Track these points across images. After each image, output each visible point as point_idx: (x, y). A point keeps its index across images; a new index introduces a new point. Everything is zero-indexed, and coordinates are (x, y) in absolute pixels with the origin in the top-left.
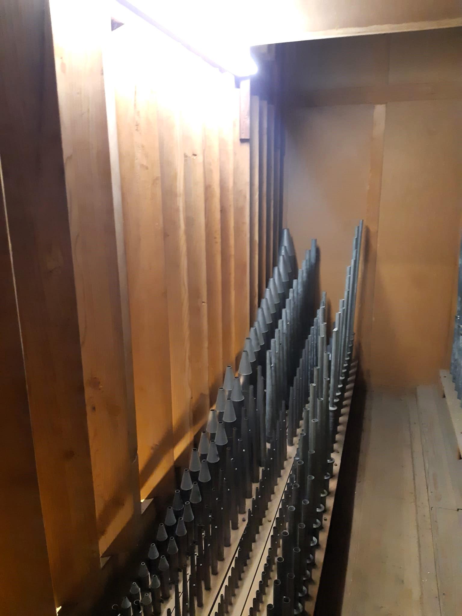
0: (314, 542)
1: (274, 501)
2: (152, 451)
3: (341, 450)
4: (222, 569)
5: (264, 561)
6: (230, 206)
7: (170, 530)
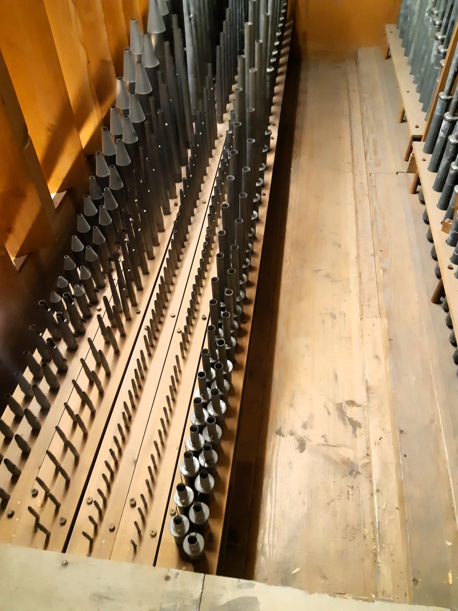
0: (254, 216)
1: (207, 183)
2: (50, 133)
3: (277, 122)
4: (159, 254)
5: (203, 240)
7: (93, 220)
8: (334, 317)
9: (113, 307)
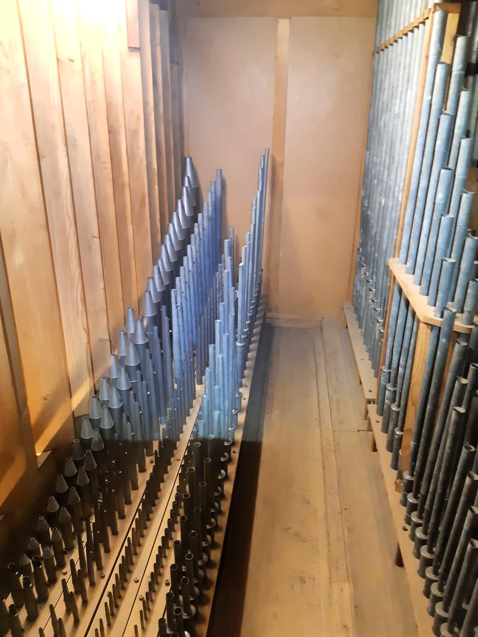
3: (249, 385)
4: (130, 513)
7: (71, 481)
8: (303, 580)
9: (79, 570)
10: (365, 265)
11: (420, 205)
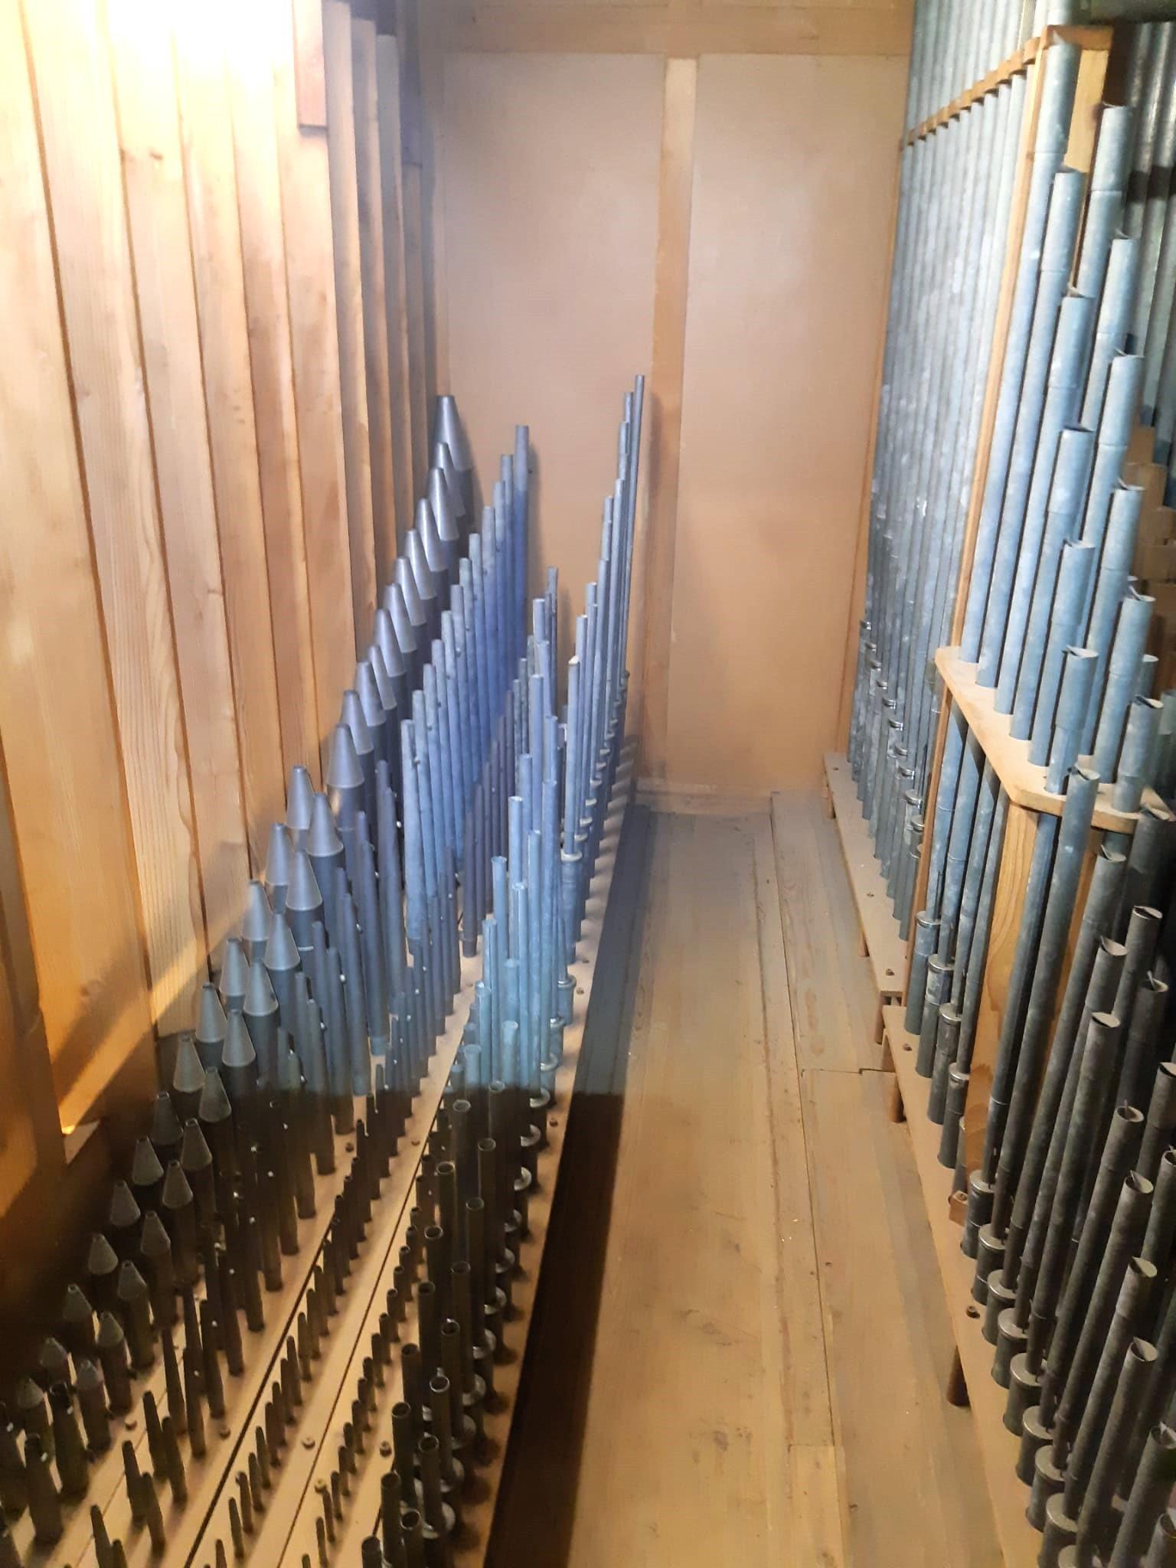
0: (523, 1181)
3: (592, 956)
6: (278, 317)
7: (147, 1196)
8: (721, 1441)
9: (166, 1420)
10: (878, 664)
11: (1011, 517)
